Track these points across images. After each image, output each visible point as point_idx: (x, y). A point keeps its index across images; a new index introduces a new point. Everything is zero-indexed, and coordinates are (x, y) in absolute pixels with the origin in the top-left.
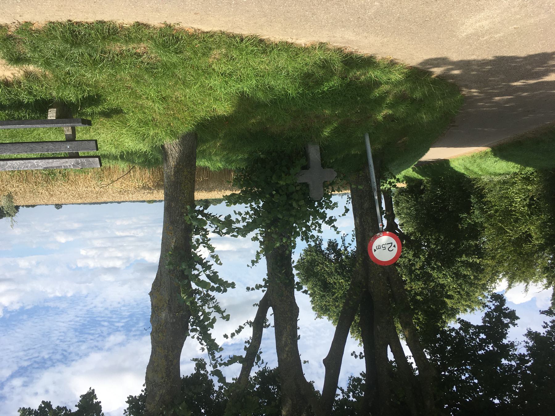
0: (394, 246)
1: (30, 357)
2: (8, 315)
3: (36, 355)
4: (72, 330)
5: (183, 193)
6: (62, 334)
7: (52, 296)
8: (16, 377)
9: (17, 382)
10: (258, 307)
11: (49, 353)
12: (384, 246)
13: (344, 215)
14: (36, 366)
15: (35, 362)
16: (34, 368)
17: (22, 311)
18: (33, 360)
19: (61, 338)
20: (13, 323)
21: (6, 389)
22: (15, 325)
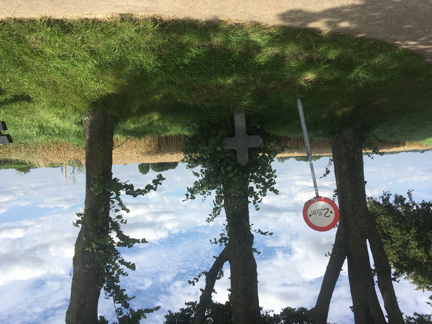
0: (331, 212)
1: (187, 267)
2: (173, 236)
3: (190, 266)
4: (214, 250)
5: (96, 162)
6: (207, 252)
7: (200, 225)
8: (178, 280)
9: (178, 284)
10: (215, 259)
11: (199, 265)
12: (319, 211)
13: (325, 175)
14: (191, 273)
15: (189, 270)
16: (189, 275)
17: (180, 235)
18: (188, 269)
19: (206, 255)
20: (177, 242)
21: (171, 288)
22: (177, 243)
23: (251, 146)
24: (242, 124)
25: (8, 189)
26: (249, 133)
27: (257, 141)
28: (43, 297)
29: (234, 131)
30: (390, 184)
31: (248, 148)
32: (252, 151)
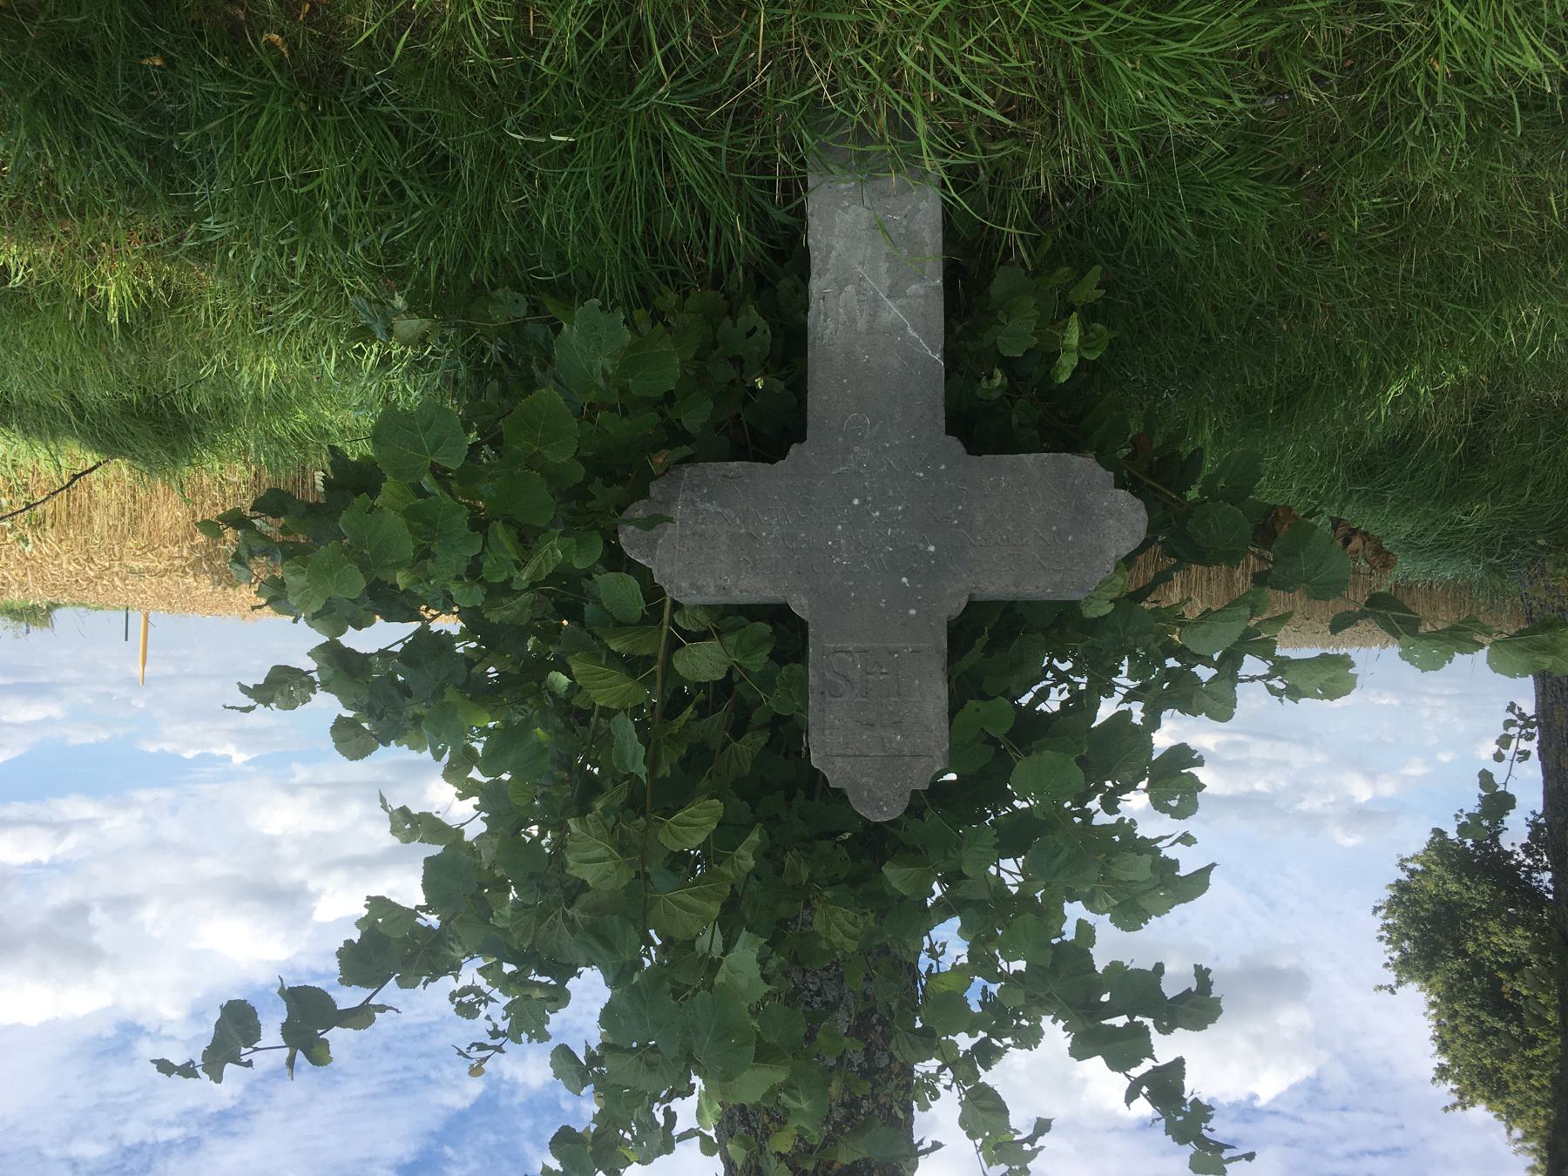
23: (997, 586)
24: (892, 311)
25: (43, 679)
26: (977, 425)
27: (1067, 526)
28: (129, 1093)
29: (798, 387)
30: (1445, 758)
31: (956, 606)
32: (991, 641)
